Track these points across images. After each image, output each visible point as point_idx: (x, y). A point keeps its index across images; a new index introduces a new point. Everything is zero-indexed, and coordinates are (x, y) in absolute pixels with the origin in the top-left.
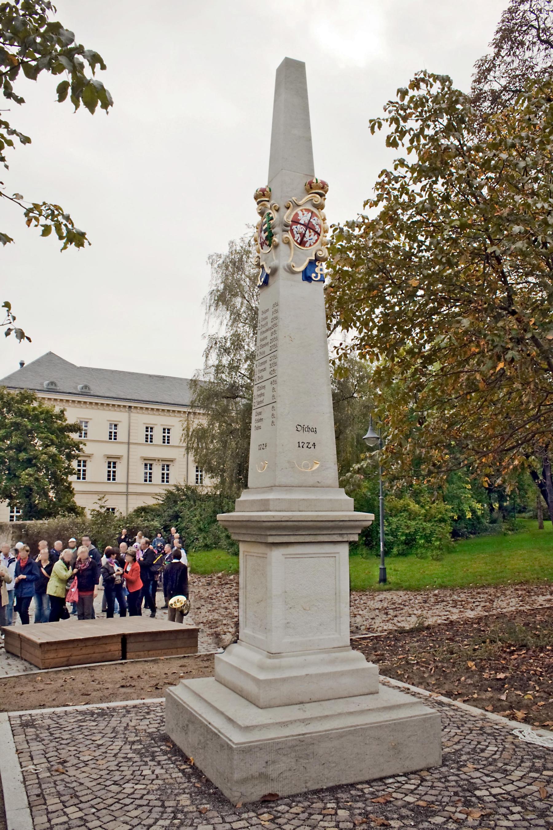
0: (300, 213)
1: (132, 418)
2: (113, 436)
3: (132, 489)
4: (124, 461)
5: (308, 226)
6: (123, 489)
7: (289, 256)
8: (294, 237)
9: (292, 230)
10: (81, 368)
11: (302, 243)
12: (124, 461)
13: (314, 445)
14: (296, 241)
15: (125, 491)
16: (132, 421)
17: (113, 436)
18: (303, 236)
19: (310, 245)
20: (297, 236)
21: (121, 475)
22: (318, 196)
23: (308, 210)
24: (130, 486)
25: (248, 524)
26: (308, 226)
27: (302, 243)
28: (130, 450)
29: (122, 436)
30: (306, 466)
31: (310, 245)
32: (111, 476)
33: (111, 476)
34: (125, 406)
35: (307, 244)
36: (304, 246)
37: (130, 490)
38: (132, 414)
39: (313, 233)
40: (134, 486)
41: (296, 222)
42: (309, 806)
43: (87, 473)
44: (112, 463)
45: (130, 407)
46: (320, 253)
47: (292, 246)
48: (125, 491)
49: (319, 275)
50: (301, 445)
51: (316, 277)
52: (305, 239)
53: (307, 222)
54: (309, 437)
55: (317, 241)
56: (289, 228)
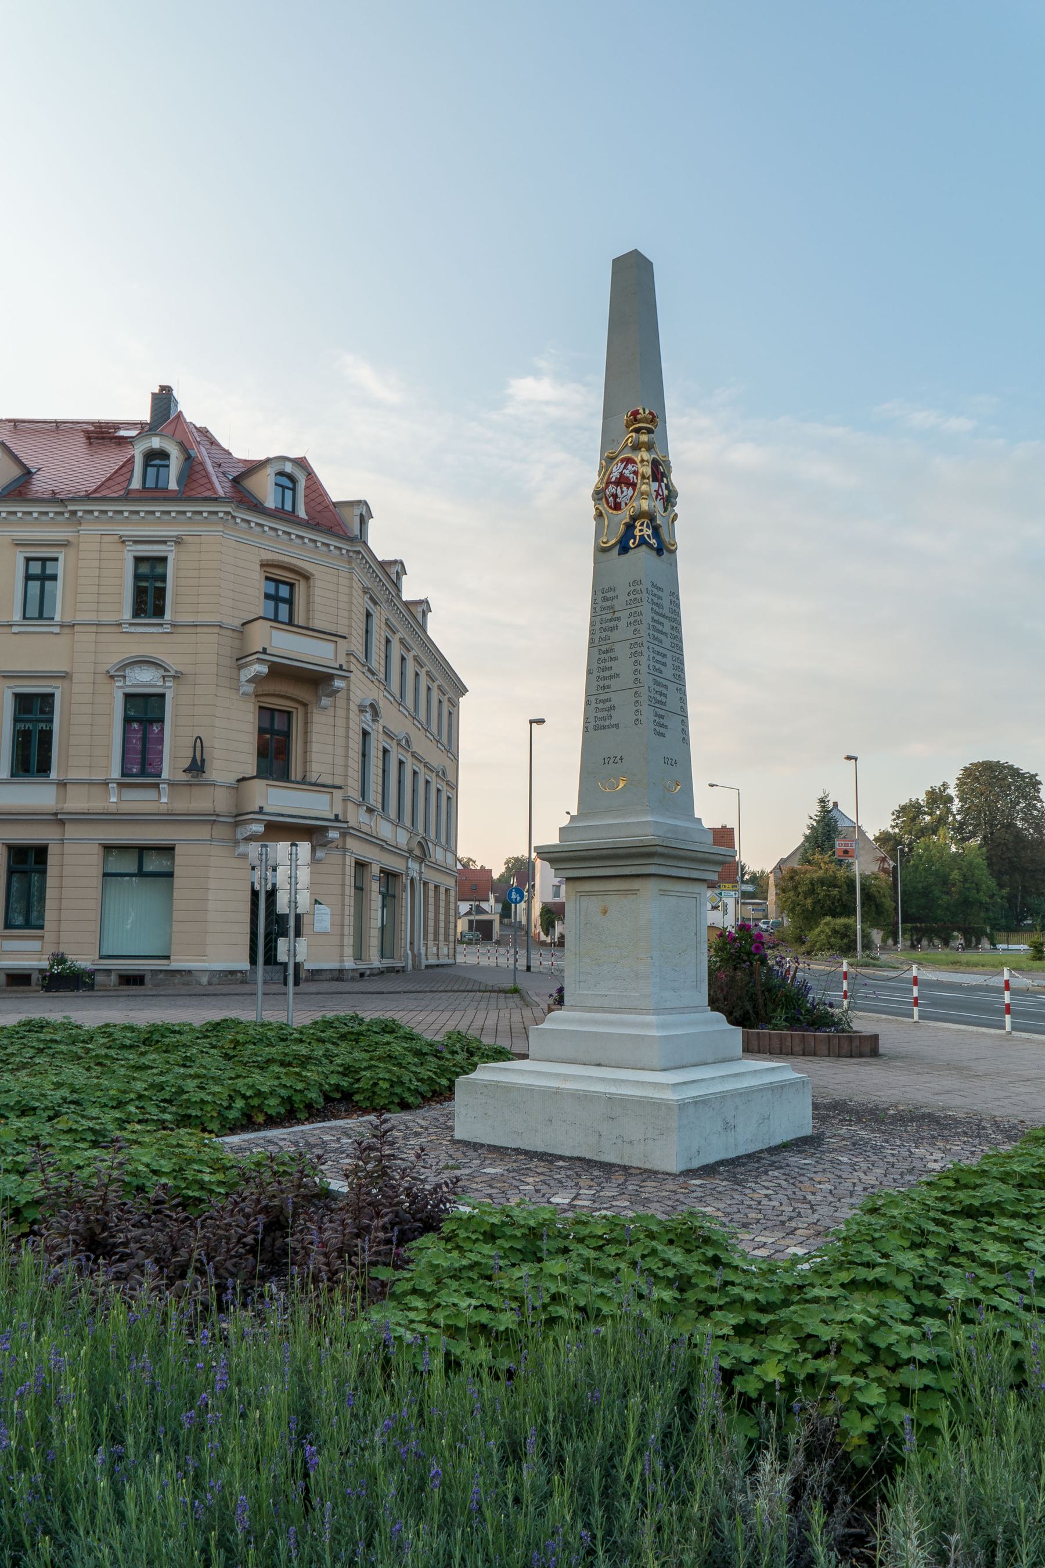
13: (621, 759)
39: (625, 489)
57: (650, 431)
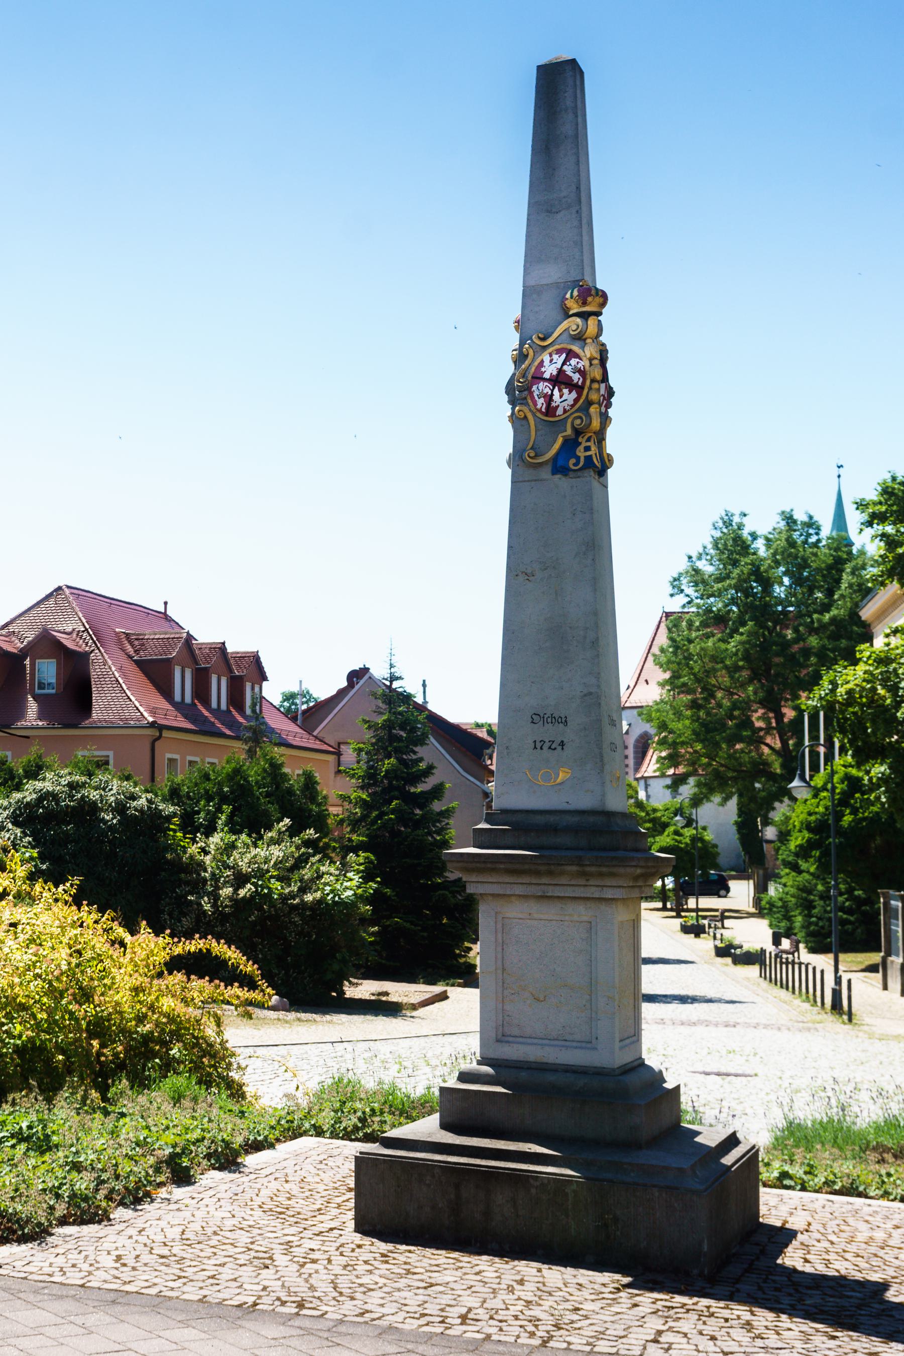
0: (546, 358)
13: (562, 744)
23: (559, 352)
39: (566, 391)
49: (582, 459)
50: (538, 745)
51: (575, 465)
52: (554, 404)
53: (555, 373)
54: (550, 732)
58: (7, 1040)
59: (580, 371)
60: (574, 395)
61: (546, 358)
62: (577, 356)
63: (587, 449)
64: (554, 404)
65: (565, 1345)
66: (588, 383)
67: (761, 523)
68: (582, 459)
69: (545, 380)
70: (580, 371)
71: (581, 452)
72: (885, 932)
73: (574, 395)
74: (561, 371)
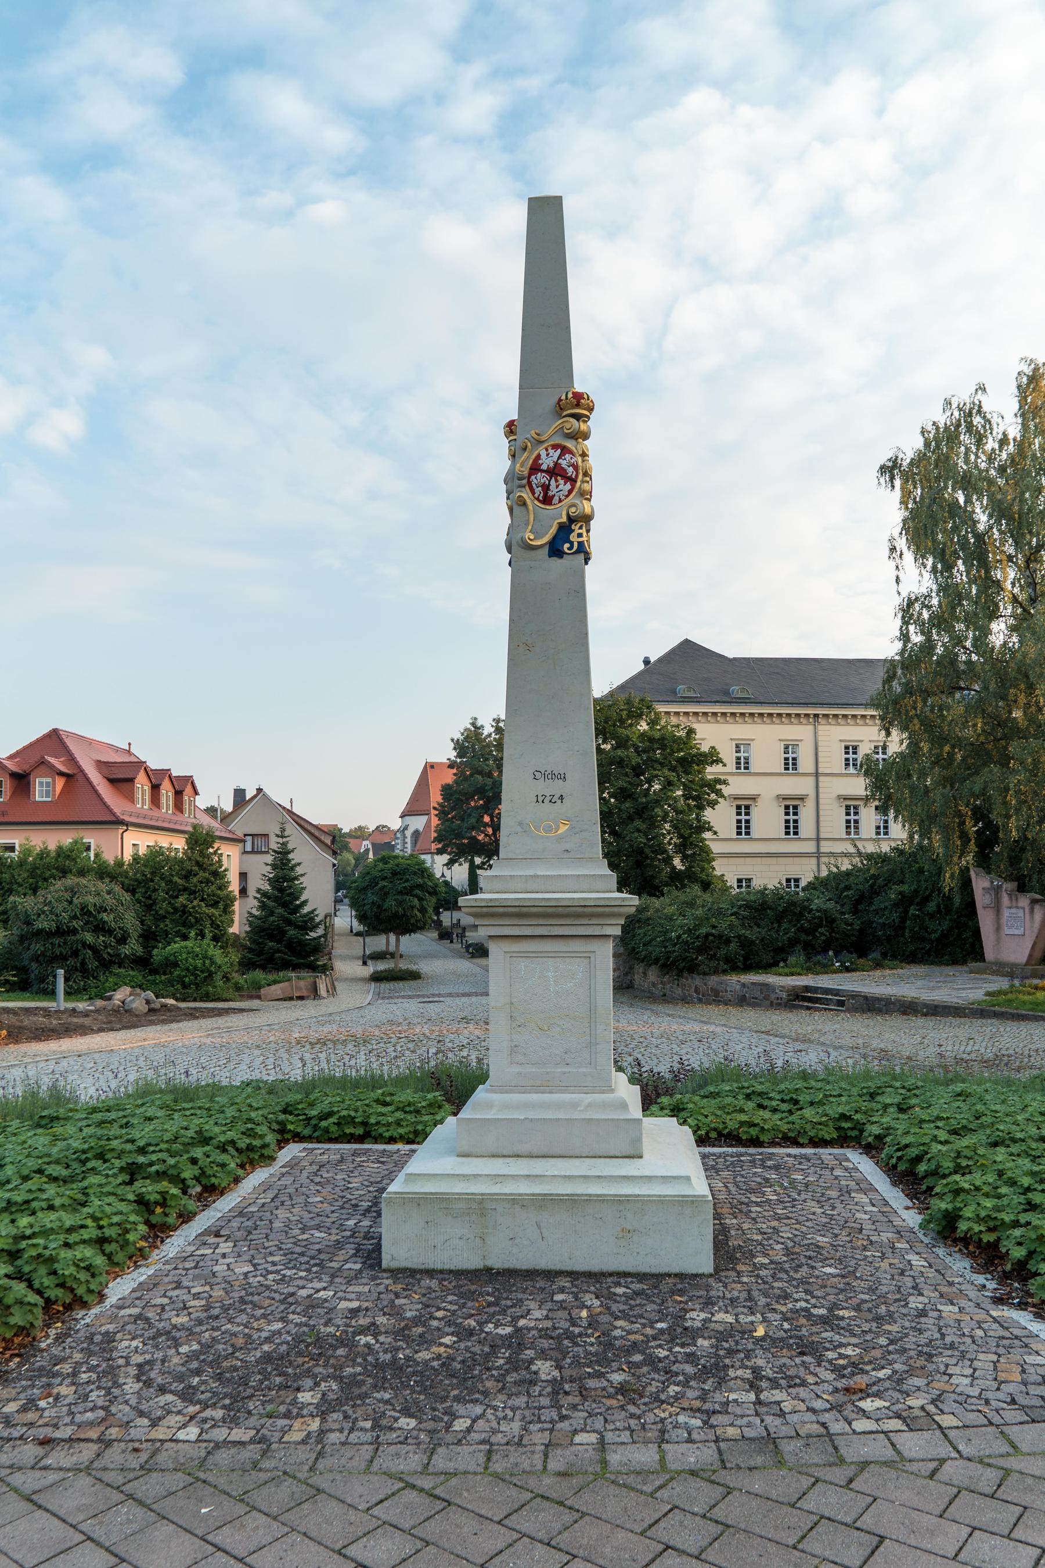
0: (543, 453)
1: (820, 733)
2: (790, 764)
3: (825, 847)
4: (810, 803)
5: (556, 471)
6: (810, 847)
7: (527, 524)
8: (533, 493)
9: (529, 483)
10: (735, 659)
11: (547, 500)
12: (810, 803)
13: (561, 798)
14: (538, 499)
15: (814, 850)
16: (820, 738)
17: (790, 764)
18: (546, 488)
19: (560, 501)
20: (538, 490)
21: (807, 828)
22: (572, 420)
23: (555, 447)
24: (822, 843)
25: (586, 910)
26: (556, 471)
27: (547, 500)
28: (821, 785)
29: (806, 764)
30: (548, 829)
31: (560, 501)
32: (792, 828)
33: (792, 828)
34: (807, 715)
35: (556, 500)
36: (550, 504)
37: (822, 850)
38: (820, 727)
39: (562, 482)
40: (830, 843)
41: (535, 469)
42: (250, 1233)
43: (752, 824)
44: (791, 807)
45: (816, 716)
46: (573, 510)
47: (531, 507)
48: (814, 850)
49: (576, 545)
50: (540, 799)
51: (570, 549)
52: (550, 493)
53: (552, 465)
54: (555, 787)
55: (570, 492)
56: (525, 482)
57: (577, 417)
58: (422, 1397)
59: (573, 465)
60: (568, 486)
61: (543, 453)
62: (571, 452)
63: (580, 535)
64: (550, 493)
65: (713, 1421)
66: (580, 477)
67: (458, 736)
68: (576, 545)
69: (543, 471)
70: (573, 465)
71: (573, 537)
72: (213, 1009)
73: (568, 486)
74: (556, 464)
